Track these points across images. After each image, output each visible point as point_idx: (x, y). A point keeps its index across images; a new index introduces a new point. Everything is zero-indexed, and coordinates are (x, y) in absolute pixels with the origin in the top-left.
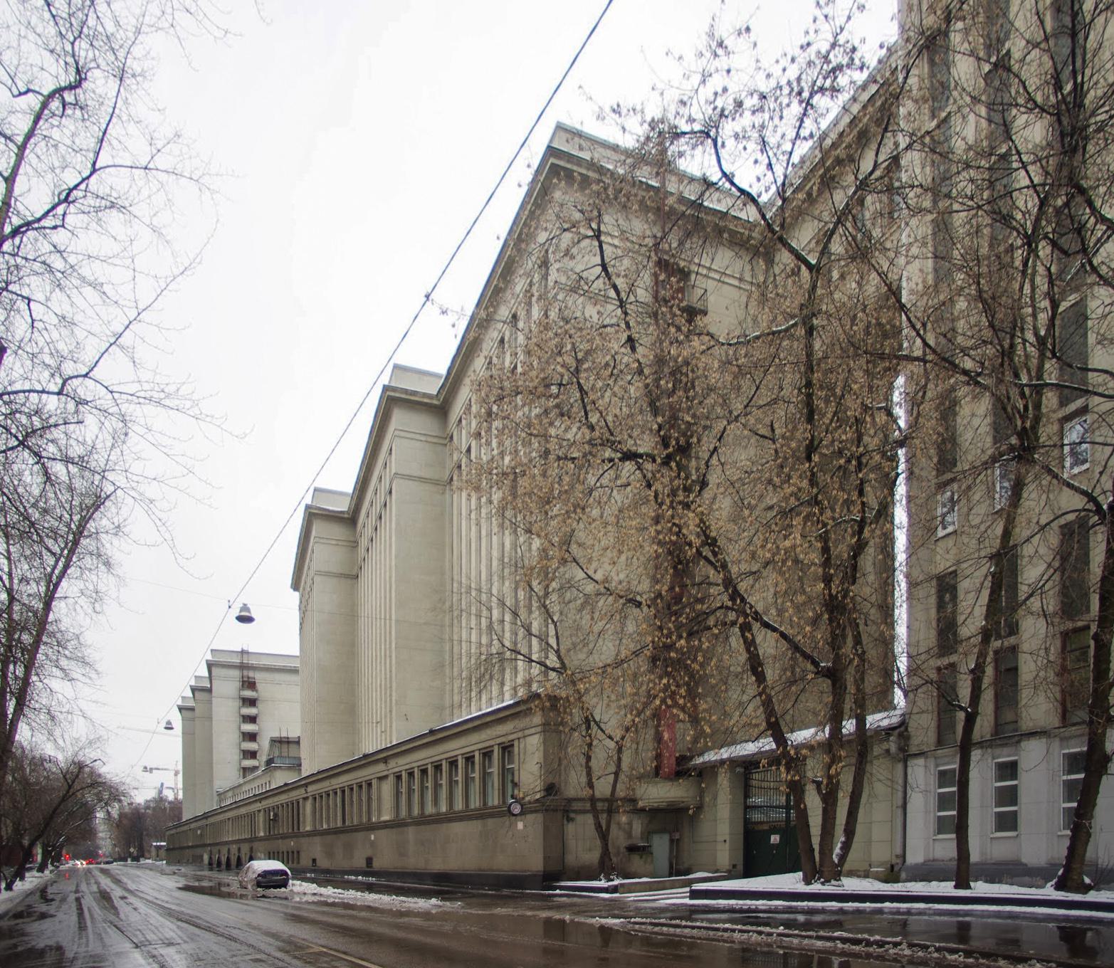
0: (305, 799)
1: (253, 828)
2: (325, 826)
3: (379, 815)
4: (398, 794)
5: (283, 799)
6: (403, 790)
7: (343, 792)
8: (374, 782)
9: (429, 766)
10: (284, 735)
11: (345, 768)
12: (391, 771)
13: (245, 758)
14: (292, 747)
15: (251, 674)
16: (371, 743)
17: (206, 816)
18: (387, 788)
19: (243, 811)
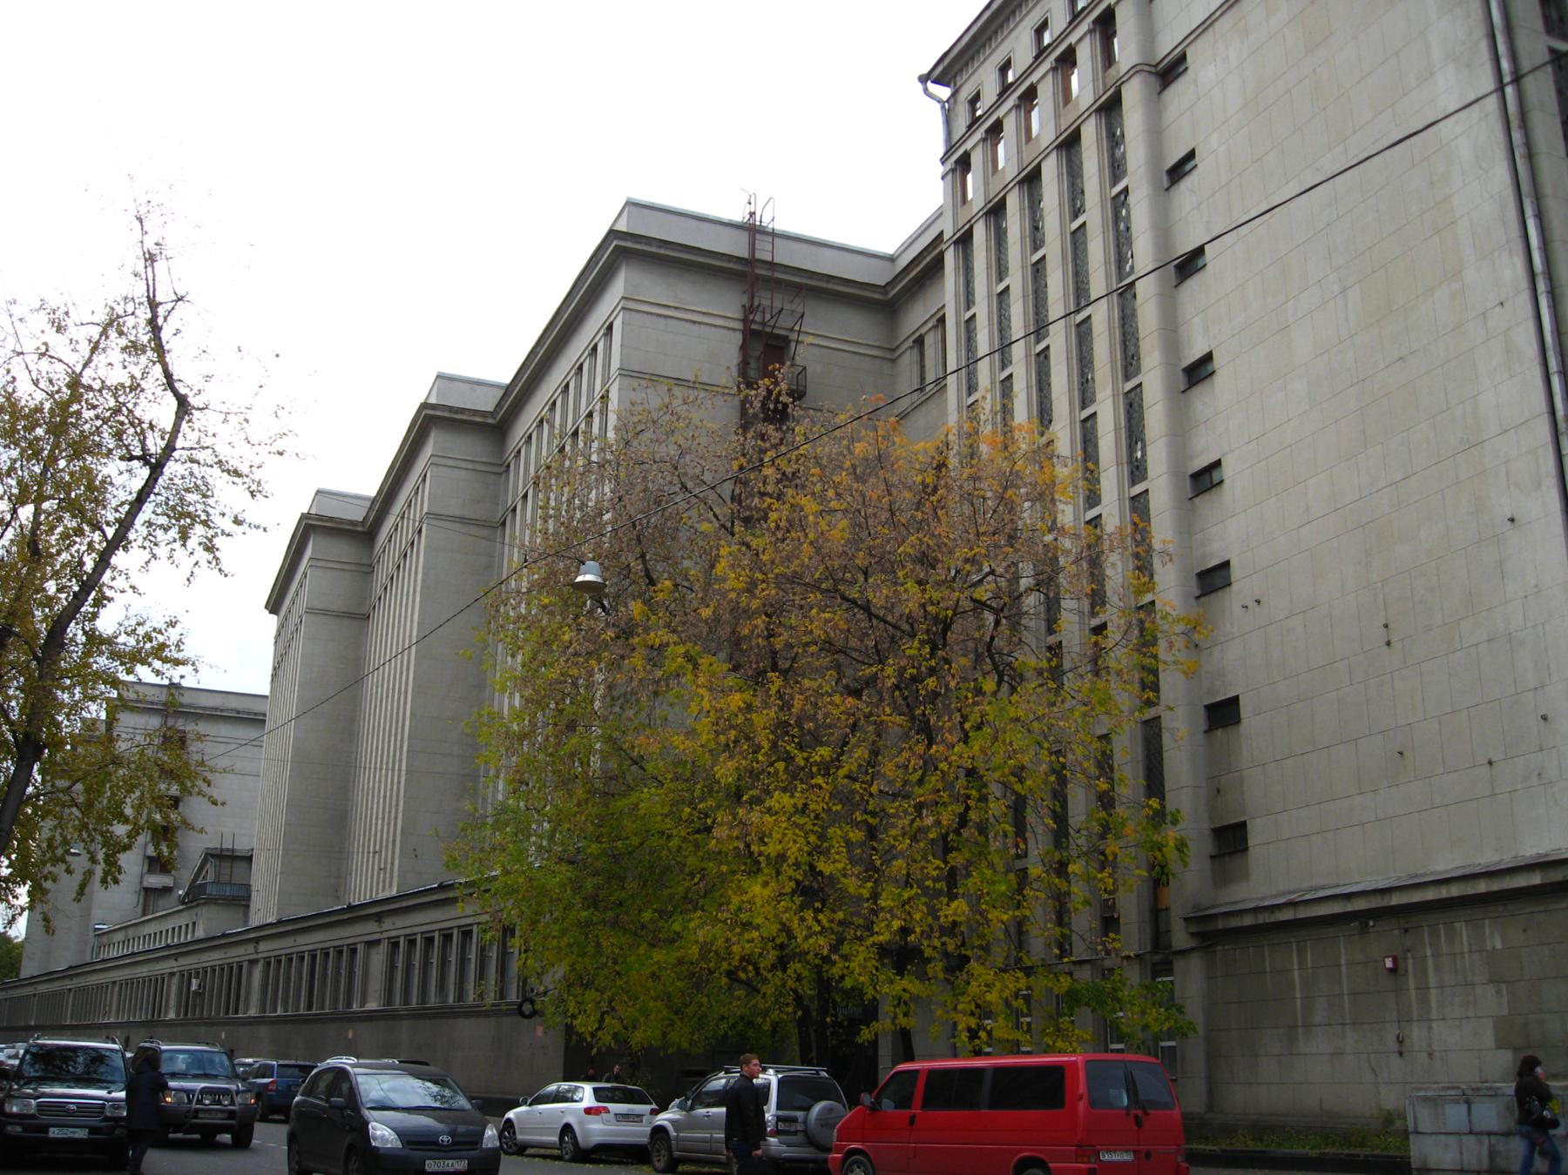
0: (253, 962)
1: (158, 1006)
2: (279, 1012)
3: (363, 1001)
4: (392, 968)
5: (215, 958)
6: (400, 964)
7: (314, 957)
8: (360, 948)
9: (436, 934)
10: (227, 845)
11: (320, 921)
12: (385, 935)
13: (150, 871)
14: (239, 867)
15: (180, 724)
16: (367, 885)
17: (72, 972)
18: (378, 958)
19: (144, 971)
